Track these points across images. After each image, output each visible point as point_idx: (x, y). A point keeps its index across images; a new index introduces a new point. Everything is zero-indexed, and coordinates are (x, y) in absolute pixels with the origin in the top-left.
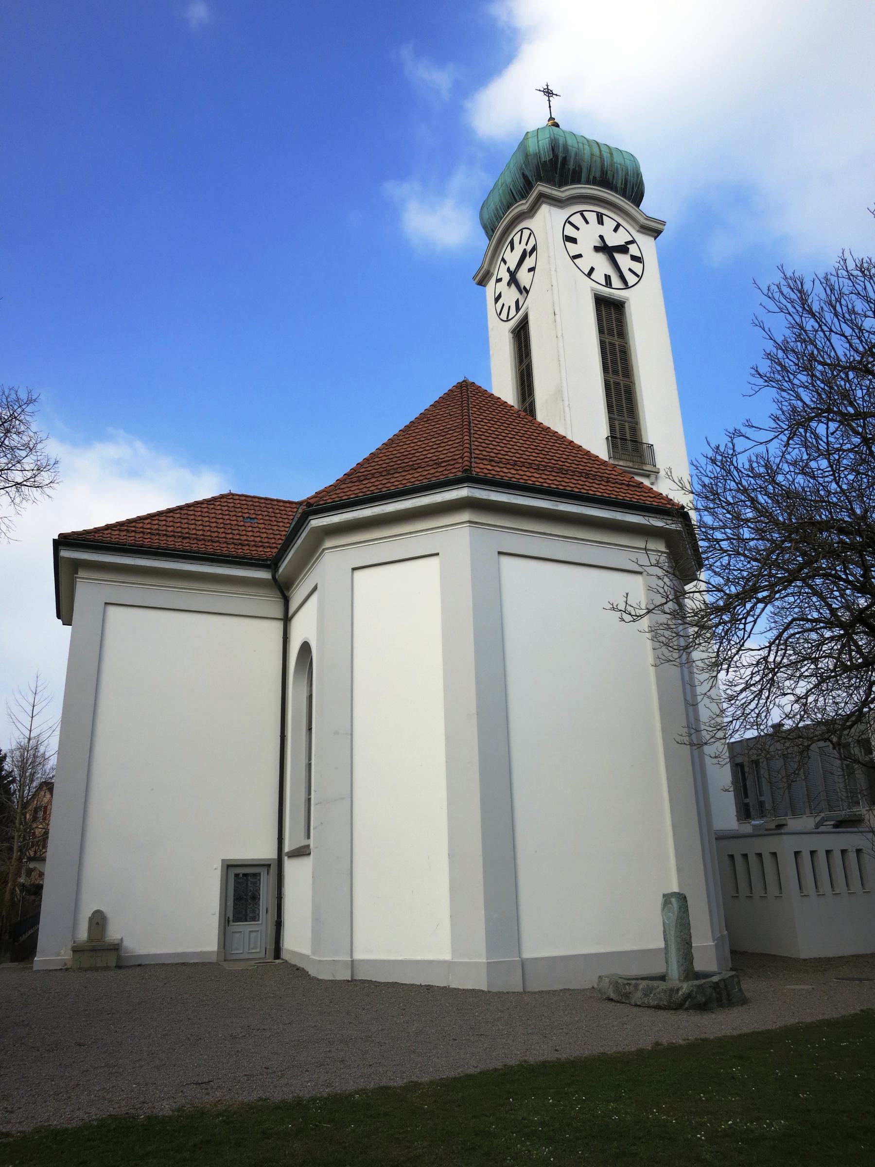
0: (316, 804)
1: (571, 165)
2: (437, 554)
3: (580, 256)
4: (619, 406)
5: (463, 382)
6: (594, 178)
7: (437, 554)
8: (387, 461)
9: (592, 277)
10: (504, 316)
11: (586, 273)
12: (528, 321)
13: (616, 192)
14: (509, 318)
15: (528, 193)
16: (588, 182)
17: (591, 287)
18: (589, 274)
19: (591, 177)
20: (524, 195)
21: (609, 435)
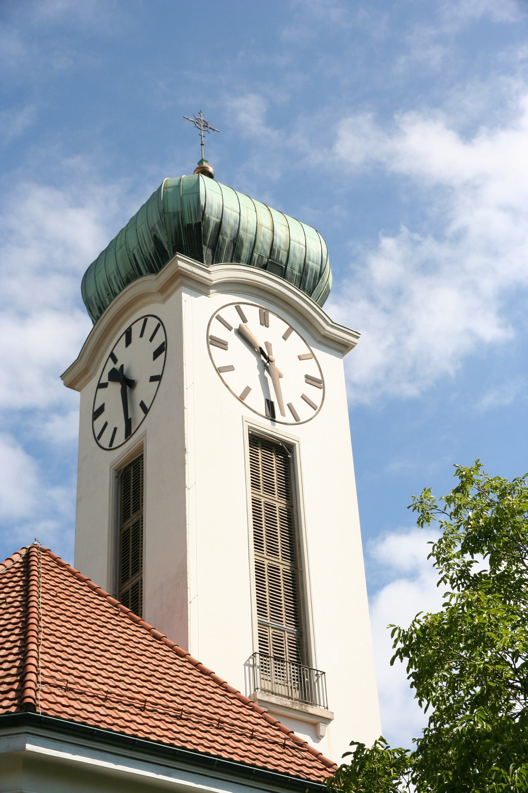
1: (228, 231)
3: (231, 368)
4: (276, 604)
10: (105, 441)
11: (238, 396)
12: (142, 455)
13: (290, 281)
14: (114, 446)
15: (161, 267)
16: (250, 262)
19: (256, 255)
21: (257, 650)
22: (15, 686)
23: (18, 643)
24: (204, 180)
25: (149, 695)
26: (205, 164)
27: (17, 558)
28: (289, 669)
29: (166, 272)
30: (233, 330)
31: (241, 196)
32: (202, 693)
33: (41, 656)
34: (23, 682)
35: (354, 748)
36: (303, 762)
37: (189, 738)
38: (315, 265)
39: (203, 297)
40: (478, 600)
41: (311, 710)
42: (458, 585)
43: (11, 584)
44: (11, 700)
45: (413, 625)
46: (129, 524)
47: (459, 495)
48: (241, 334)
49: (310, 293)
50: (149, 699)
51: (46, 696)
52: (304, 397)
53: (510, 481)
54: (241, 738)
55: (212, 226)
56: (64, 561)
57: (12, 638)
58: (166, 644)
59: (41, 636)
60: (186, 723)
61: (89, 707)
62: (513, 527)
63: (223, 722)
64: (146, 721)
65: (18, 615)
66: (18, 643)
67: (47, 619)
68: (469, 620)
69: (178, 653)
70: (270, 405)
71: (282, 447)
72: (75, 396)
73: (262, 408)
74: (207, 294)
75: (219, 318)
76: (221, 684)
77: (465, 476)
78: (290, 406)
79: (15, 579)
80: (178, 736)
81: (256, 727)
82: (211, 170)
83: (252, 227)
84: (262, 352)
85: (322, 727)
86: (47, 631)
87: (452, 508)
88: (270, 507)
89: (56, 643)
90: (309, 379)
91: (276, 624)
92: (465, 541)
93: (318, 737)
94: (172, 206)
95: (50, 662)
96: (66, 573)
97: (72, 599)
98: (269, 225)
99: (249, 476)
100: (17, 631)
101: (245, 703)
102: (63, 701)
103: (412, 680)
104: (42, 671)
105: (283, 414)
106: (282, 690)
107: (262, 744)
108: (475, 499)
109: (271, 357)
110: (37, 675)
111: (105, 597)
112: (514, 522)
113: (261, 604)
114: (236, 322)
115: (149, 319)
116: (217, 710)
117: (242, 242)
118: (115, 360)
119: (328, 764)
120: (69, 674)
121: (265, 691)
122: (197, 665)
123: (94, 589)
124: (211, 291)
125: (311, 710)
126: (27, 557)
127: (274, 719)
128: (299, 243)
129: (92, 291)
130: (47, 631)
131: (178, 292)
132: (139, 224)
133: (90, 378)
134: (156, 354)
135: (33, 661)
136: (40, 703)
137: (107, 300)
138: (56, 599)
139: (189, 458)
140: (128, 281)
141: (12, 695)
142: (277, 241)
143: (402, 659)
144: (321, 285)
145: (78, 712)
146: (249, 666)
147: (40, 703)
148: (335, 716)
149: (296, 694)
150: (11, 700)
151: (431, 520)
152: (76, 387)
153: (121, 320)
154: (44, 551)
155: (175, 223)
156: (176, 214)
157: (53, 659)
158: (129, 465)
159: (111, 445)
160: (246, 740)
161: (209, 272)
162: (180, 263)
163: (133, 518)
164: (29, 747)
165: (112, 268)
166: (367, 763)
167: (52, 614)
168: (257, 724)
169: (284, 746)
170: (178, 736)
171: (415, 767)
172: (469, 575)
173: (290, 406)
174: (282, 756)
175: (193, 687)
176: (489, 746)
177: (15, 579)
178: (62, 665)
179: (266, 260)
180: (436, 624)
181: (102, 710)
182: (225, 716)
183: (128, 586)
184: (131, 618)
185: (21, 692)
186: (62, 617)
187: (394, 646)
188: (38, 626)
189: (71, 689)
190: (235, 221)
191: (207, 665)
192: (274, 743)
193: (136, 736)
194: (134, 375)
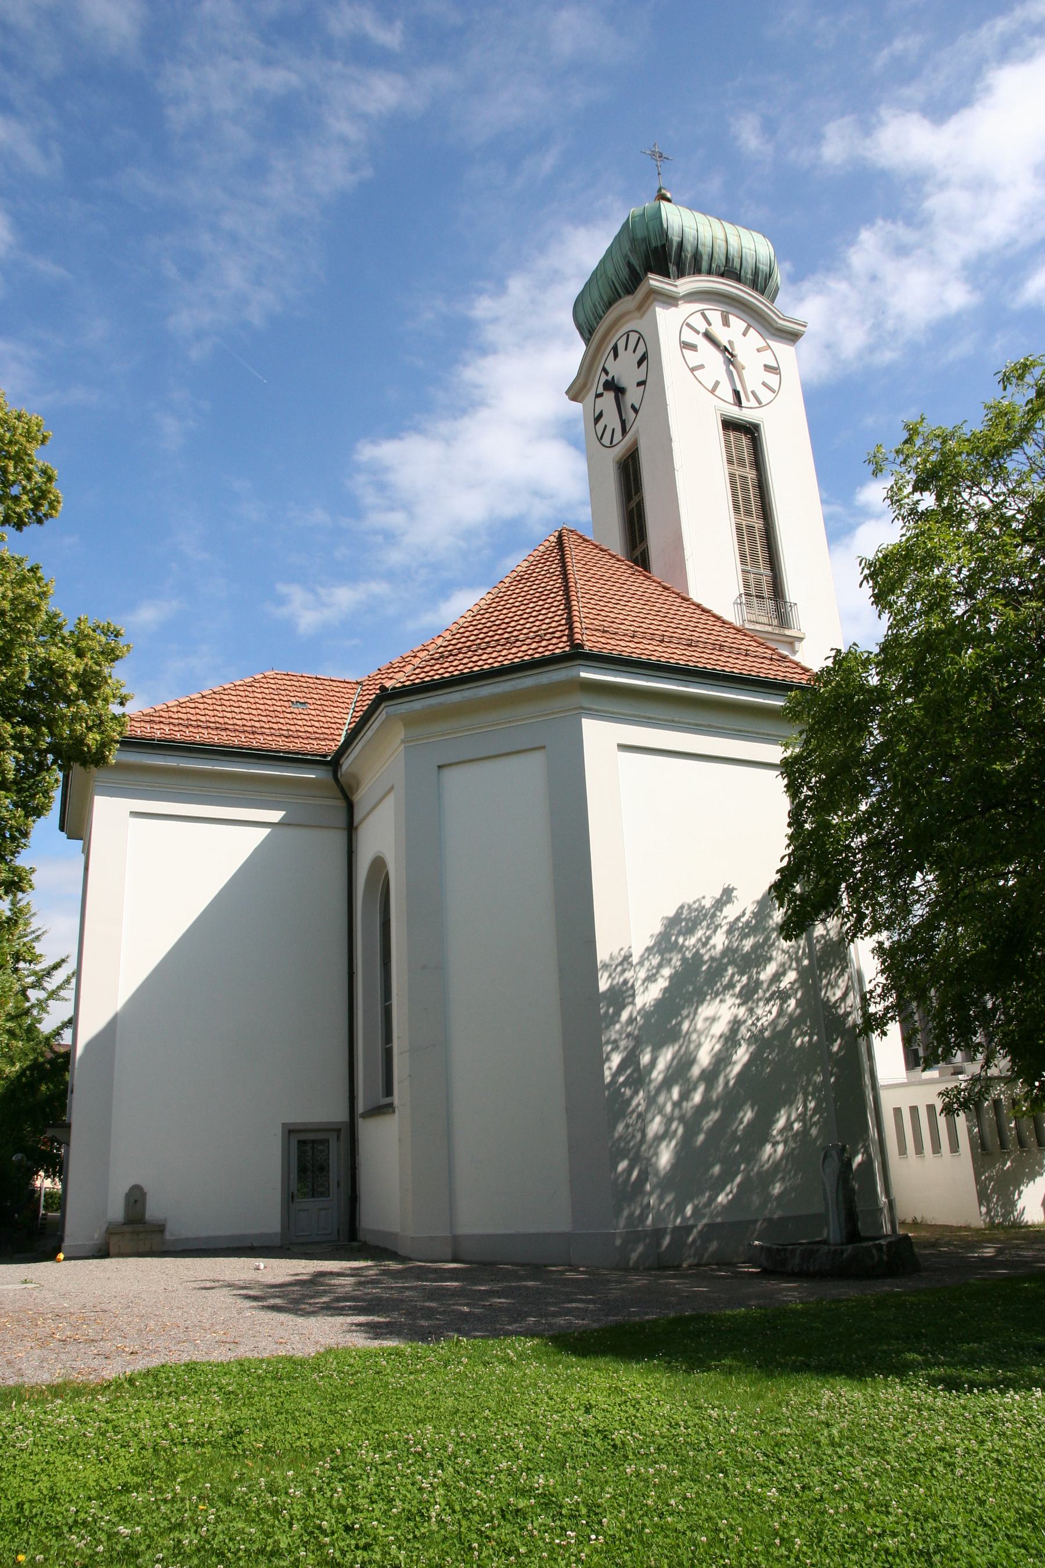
0: (402, 1053)
1: (689, 248)
2: (544, 747)
3: (702, 367)
5: (793, 789)
6: (718, 266)
7: (544, 747)
8: (476, 632)
9: (716, 393)
10: (606, 440)
11: (710, 389)
12: (637, 449)
13: (745, 284)
14: (614, 444)
15: (636, 288)
16: (709, 272)
17: (696, 351)
18: (713, 391)
19: (714, 266)
20: (630, 290)
21: (742, 591)
22: (566, 632)
23: (563, 602)
24: (664, 204)
25: (666, 631)
26: (663, 191)
27: (552, 539)
28: (770, 604)
29: (641, 292)
30: (701, 334)
31: (697, 214)
32: (705, 626)
33: (581, 609)
34: (571, 629)
35: (833, 653)
36: (787, 670)
37: (699, 660)
38: (765, 267)
39: (674, 309)
40: (929, 529)
41: (788, 632)
42: (909, 521)
43: (551, 559)
44: (564, 642)
45: (877, 555)
46: (633, 504)
47: (907, 446)
48: (708, 336)
49: (762, 293)
50: (665, 634)
51: (590, 638)
52: (764, 384)
53: (950, 429)
54: (738, 656)
55: (675, 245)
56: (587, 537)
57: (559, 598)
58: (673, 593)
59: (579, 595)
60: (695, 649)
61: (622, 643)
62: (955, 467)
63: (723, 646)
64: (665, 649)
65: (560, 581)
66: (563, 602)
67: (582, 582)
68: (922, 546)
69: (684, 599)
70: (737, 394)
71: (749, 428)
72: (577, 407)
73: (730, 398)
74: (676, 306)
75: (688, 325)
76: (718, 618)
77: (912, 429)
78: (753, 393)
79: (553, 555)
80: (690, 658)
81: (749, 648)
82: (669, 195)
83: (708, 242)
84: (726, 349)
85: (797, 644)
86: (582, 591)
87: (901, 458)
88: (744, 478)
89: (591, 599)
90: (768, 368)
91: (755, 570)
92: (915, 483)
93: (794, 652)
94: (640, 234)
95: (589, 613)
96: (590, 547)
97: (598, 565)
98: (723, 237)
99: (724, 455)
100: (561, 593)
101: (738, 630)
102: (603, 640)
103: (872, 599)
104: (584, 620)
105: (748, 400)
106: (765, 620)
107: (754, 659)
108: (920, 448)
109: (734, 353)
110: (581, 623)
111: (623, 561)
112: (956, 462)
113: (743, 556)
114: (702, 327)
115: (631, 334)
116: (718, 638)
117: (701, 256)
118: (607, 373)
119: (806, 670)
120: (604, 621)
121: (751, 622)
122: (698, 606)
123: (614, 556)
124: (680, 302)
125: (788, 632)
126: (560, 537)
127: (762, 641)
128: (750, 249)
129: (582, 318)
130: (582, 591)
131: (651, 309)
132: (614, 253)
133: (589, 391)
134: (640, 363)
135: (577, 613)
136: (586, 643)
137: (595, 323)
138: (586, 567)
139: (675, 445)
140: (610, 304)
141: (565, 639)
142: (731, 251)
143: (868, 582)
144: (772, 284)
145: (615, 647)
146: (737, 604)
147: (586, 643)
148: (806, 635)
149: (775, 622)
150: (564, 642)
151: (884, 471)
152: (579, 400)
153: (607, 341)
154: (572, 531)
155: (643, 247)
156: (644, 240)
157: (591, 611)
158: (628, 457)
159: (611, 443)
160: (742, 658)
161: (676, 286)
162: (652, 282)
163: (636, 499)
164: (583, 675)
165: (596, 295)
166: (844, 663)
167: (584, 578)
168: (749, 645)
169: (771, 659)
170: (690, 658)
171: (878, 664)
172: (917, 512)
173: (753, 393)
174: (770, 667)
175: (698, 623)
176: (943, 640)
177: (553, 555)
178: (598, 615)
179: (722, 269)
180: (895, 551)
181: (632, 645)
182: (724, 642)
183: (638, 552)
184: (644, 576)
185: (571, 636)
186: (592, 580)
187: (862, 573)
188: (576, 588)
189: (607, 631)
190: (694, 238)
191: (706, 605)
192: (764, 658)
193: (660, 661)
194: (624, 383)
